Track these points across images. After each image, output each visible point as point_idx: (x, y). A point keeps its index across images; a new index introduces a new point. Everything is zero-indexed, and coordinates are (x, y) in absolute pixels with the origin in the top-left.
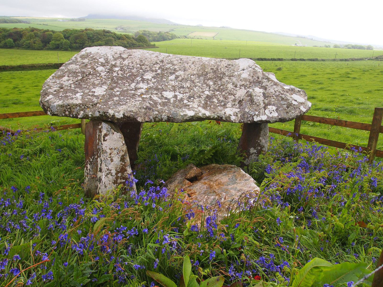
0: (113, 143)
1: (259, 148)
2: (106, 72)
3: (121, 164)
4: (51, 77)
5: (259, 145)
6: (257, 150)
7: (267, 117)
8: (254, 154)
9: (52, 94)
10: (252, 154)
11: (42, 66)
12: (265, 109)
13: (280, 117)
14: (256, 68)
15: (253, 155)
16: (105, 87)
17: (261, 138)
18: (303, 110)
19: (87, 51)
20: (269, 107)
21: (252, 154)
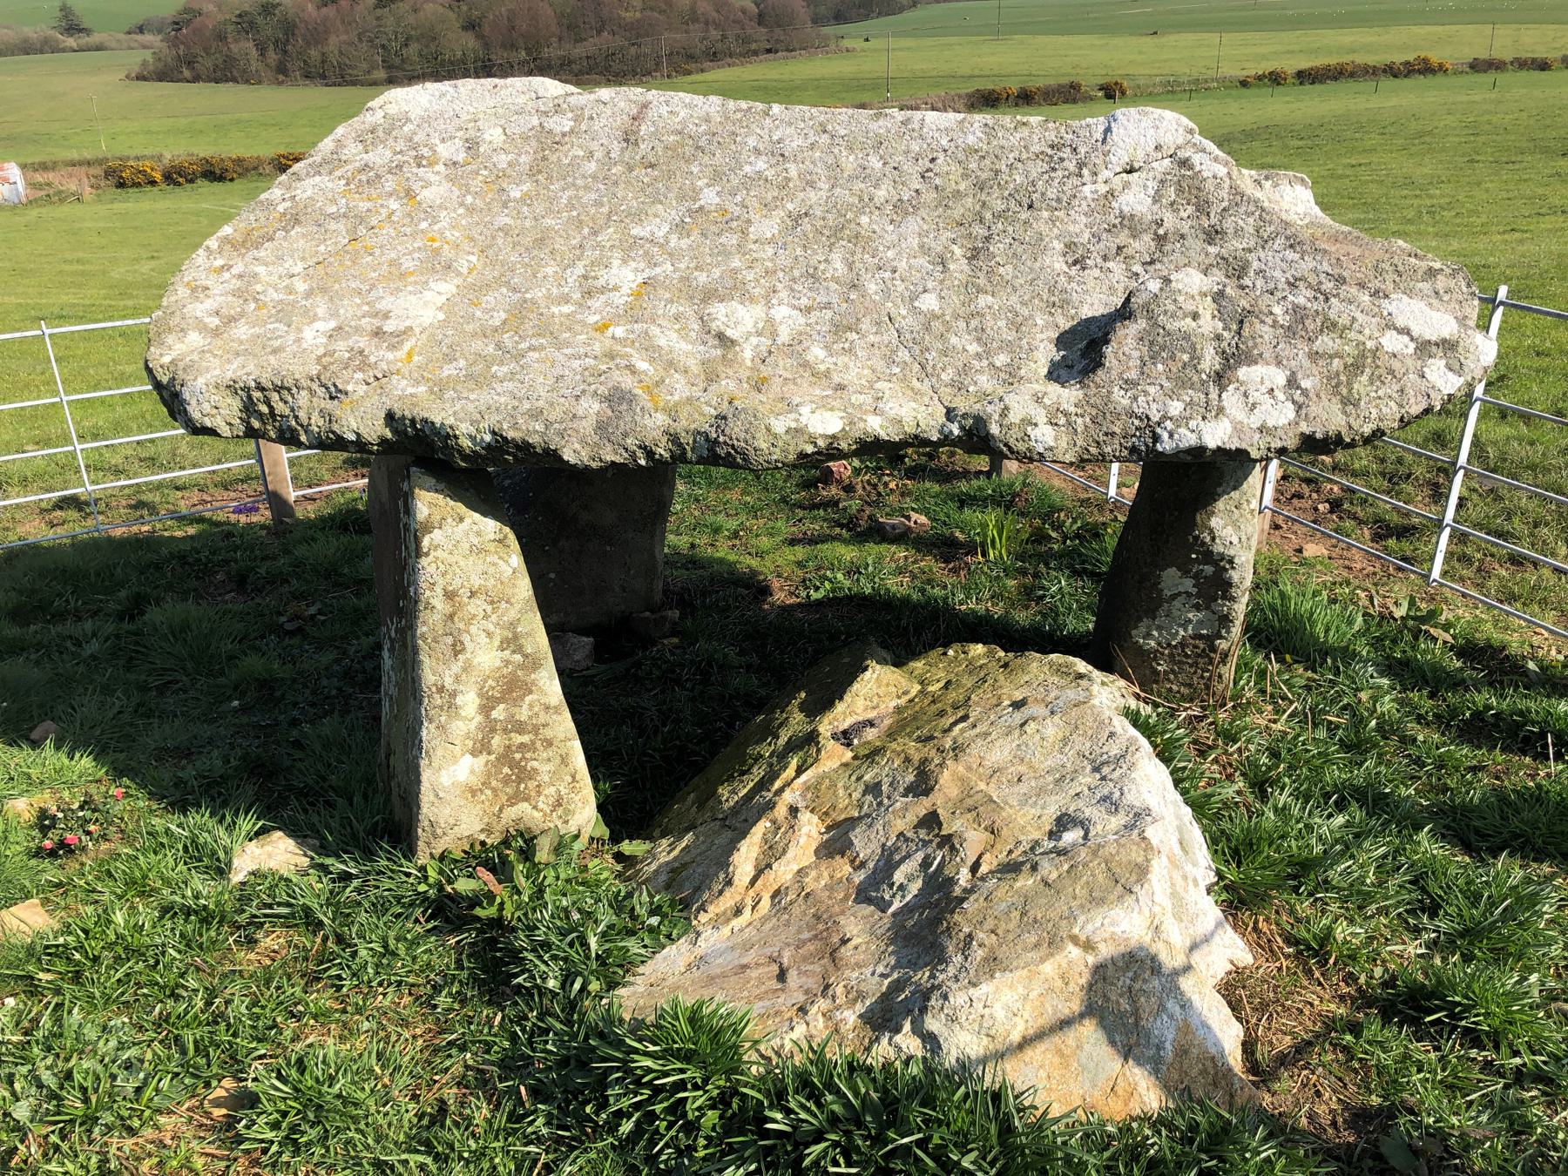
0: (469, 562)
1: (1209, 569)
2: (461, 211)
3: (507, 663)
4: (213, 243)
5: (1208, 556)
6: (1196, 576)
7: (1229, 430)
8: (1182, 599)
9: (202, 328)
10: (1174, 597)
11: (1352, 75)
12: (1222, 389)
13: (1304, 428)
14: (1196, 159)
15: (1177, 604)
16: (444, 288)
17: (1215, 522)
18: (1439, 384)
19: (392, 109)
20: (1243, 372)
21: (1174, 597)
